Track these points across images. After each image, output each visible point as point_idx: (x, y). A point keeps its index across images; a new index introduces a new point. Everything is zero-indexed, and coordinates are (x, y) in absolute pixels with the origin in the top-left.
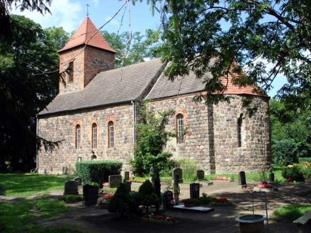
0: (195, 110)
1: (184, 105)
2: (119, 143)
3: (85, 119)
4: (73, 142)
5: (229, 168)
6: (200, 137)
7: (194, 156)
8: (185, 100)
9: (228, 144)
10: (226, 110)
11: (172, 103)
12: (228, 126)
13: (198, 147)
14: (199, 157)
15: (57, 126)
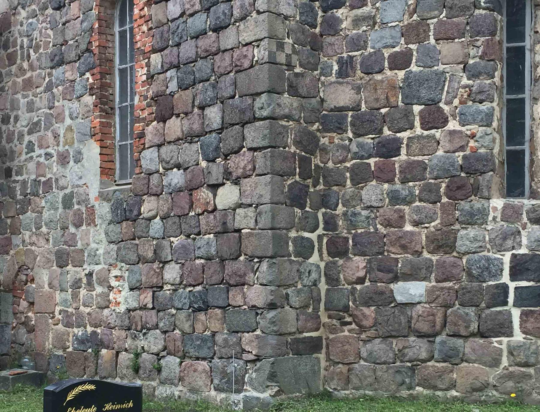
5: (418, 347)
6: (216, 123)
13: (204, 194)
14: (213, 273)
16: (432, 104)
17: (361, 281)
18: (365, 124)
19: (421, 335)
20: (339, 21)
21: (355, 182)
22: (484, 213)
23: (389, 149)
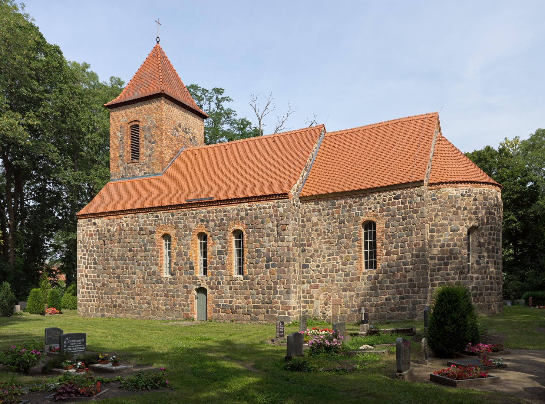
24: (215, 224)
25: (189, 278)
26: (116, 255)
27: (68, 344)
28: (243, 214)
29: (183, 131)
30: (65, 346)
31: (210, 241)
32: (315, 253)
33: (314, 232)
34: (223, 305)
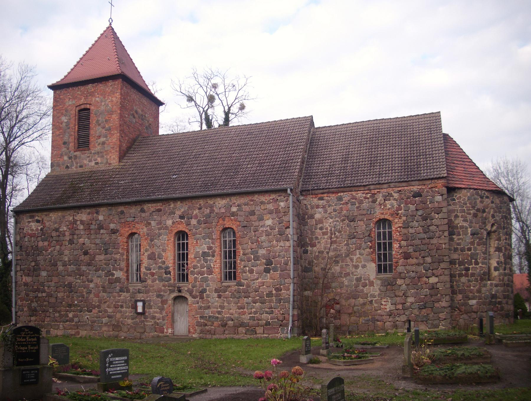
0: (420, 213)
1: (395, 203)
2: (251, 271)
3: (153, 223)
4: (121, 270)
7: (415, 296)
8: (396, 195)
9: (473, 275)
10: (470, 216)
11: (365, 198)
12: (472, 243)
13: (424, 279)
15: (73, 234)
16: (476, 260)
17: (460, 300)
18: (461, 263)
19: (474, 312)
20: (454, 239)
21: (459, 277)
22: (486, 284)
23: (467, 269)
24: (199, 221)
25: (164, 286)
26: (66, 259)
27: (111, 363)
28: (234, 209)
29: (139, 117)
30: (107, 365)
31: (191, 241)
32: (320, 255)
33: (318, 231)
34: (210, 317)
